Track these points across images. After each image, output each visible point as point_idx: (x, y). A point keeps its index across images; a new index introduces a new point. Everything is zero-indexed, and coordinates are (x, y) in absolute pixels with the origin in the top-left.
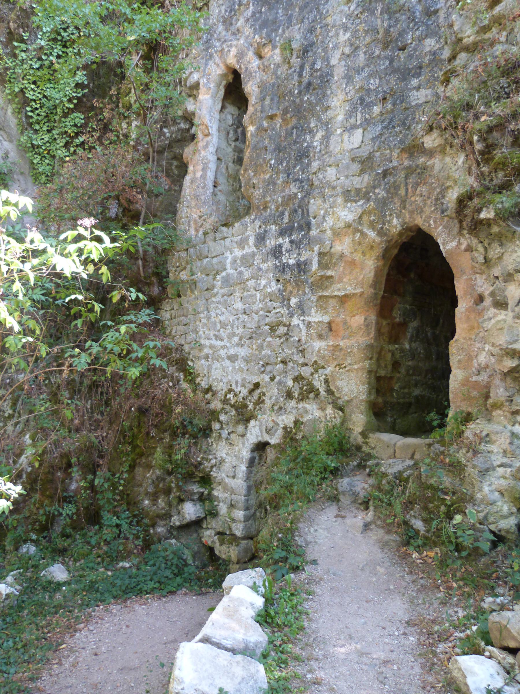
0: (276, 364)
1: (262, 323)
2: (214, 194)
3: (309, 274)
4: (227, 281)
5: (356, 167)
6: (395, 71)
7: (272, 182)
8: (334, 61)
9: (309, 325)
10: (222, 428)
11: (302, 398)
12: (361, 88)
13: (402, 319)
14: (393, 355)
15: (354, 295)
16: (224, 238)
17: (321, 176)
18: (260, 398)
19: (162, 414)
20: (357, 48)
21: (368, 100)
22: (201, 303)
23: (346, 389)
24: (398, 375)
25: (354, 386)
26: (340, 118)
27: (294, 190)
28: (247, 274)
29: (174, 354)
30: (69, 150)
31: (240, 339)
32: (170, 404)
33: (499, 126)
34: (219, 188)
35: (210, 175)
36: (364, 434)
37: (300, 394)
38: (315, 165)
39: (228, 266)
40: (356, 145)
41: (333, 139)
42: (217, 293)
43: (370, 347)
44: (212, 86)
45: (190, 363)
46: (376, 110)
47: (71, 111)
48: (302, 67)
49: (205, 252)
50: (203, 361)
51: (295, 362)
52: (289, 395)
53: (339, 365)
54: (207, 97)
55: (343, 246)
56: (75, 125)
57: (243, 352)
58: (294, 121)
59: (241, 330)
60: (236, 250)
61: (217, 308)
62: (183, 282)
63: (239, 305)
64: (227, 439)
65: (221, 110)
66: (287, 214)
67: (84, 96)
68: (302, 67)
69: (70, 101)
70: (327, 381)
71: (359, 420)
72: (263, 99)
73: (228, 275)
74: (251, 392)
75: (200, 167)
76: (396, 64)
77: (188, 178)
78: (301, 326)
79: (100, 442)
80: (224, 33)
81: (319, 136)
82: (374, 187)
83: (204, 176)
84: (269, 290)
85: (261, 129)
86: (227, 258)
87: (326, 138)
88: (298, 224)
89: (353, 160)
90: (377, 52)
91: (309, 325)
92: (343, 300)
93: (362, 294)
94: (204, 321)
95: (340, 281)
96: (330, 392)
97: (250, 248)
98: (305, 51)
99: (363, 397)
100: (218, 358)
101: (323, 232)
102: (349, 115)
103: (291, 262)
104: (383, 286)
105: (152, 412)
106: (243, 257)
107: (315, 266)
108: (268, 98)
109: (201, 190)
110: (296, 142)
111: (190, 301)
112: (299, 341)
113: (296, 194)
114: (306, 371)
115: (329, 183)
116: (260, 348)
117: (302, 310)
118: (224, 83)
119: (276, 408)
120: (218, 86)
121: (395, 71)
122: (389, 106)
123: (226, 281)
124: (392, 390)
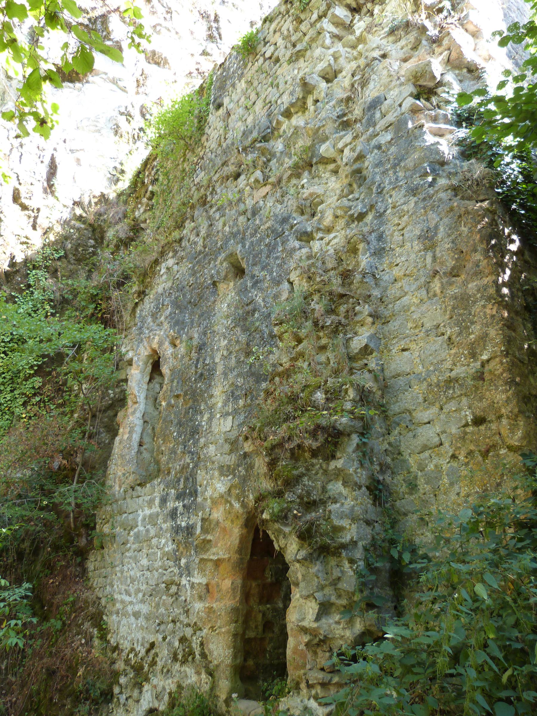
0: (168, 623)
1: (160, 581)
2: (139, 452)
3: (195, 537)
4: (138, 537)
5: (227, 447)
6: (253, 374)
7: (173, 451)
8: (217, 360)
9: (192, 586)
10: (121, 693)
11: (184, 662)
12: (233, 383)
13: (274, 579)
14: (264, 615)
15: (224, 559)
16: (139, 497)
17: (205, 451)
18: (153, 659)
19: (68, 677)
20: (231, 352)
21: (237, 393)
22: (118, 556)
23: (215, 653)
24: (270, 635)
25: (221, 650)
26: (220, 405)
27: (188, 460)
28: (152, 533)
29: (90, 609)
30: (26, 408)
31: (144, 596)
32: (77, 665)
33: (280, 445)
34: (144, 447)
35: (136, 437)
36: (228, 701)
37: (183, 656)
38: (202, 440)
39: (140, 523)
40: (228, 429)
41: (215, 422)
42: (130, 548)
43: (235, 610)
44: (141, 364)
45: (105, 617)
46: (241, 402)
47: (31, 376)
48: (198, 360)
49: (124, 509)
50: (114, 617)
51: (181, 622)
52: (175, 658)
53: (212, 627)
54: (137, 372)
55: (218, 514)
56: (33, 388)
57: (144, 609)
58: (190, 403)
59: (145, 586)
60: (146, 508)
61: (129, 563)
62: (105, 535)
63: (145, 562)
64: (124, 705)
65: (150, 380)
66: (182, 480)
67: (44, 363)
68: (198, 360)
69: (32, 367)
70: (202, 644)
71: (224, 685)
72: (172, 381)
73: (139, 531)
74: (148, 651)
75: (128, 430)
76: (253, 370)
77: (117, 439)
78: (187, 586)
79: (7, 709)
80: (151, 324)
81: (206, 417)
82: (238, 466)
83: (130, 438)
84: (167, 549)
85: (169, 405)
86: (139, 515)
87: (210, 419)
88: (189, 492)
89: (226, 440)
90: (242, 359)
91: (192, 586)
92: (217, 563)
93: (229, 559)
94: (119, 574)
95: (216, 546)
96: (204, 655)
97: (156, 509)
98: (200, 348)
99: (228, 661)
100: (126, 615)
101: (205, 499)
102: (225, 404)
103: (183, 524)
104: (249, 551)
105: (58, 674)
106: (151, 516)
107: (198, 531)
108: (176, 381)
109: (126, 450)
110: (191, 420)
111: (112, 553)
112: (186, 601)
113: (189, 464)
114: (188, 632)
115: (210, 458)
116: (158, 606)
117: (188, 570)
118: (151, 361)
119: (165, 670)
120: (146, 364)
121: (253, 374)
122: (249, 401)
123: (137, 536)
124: (264, 651)
